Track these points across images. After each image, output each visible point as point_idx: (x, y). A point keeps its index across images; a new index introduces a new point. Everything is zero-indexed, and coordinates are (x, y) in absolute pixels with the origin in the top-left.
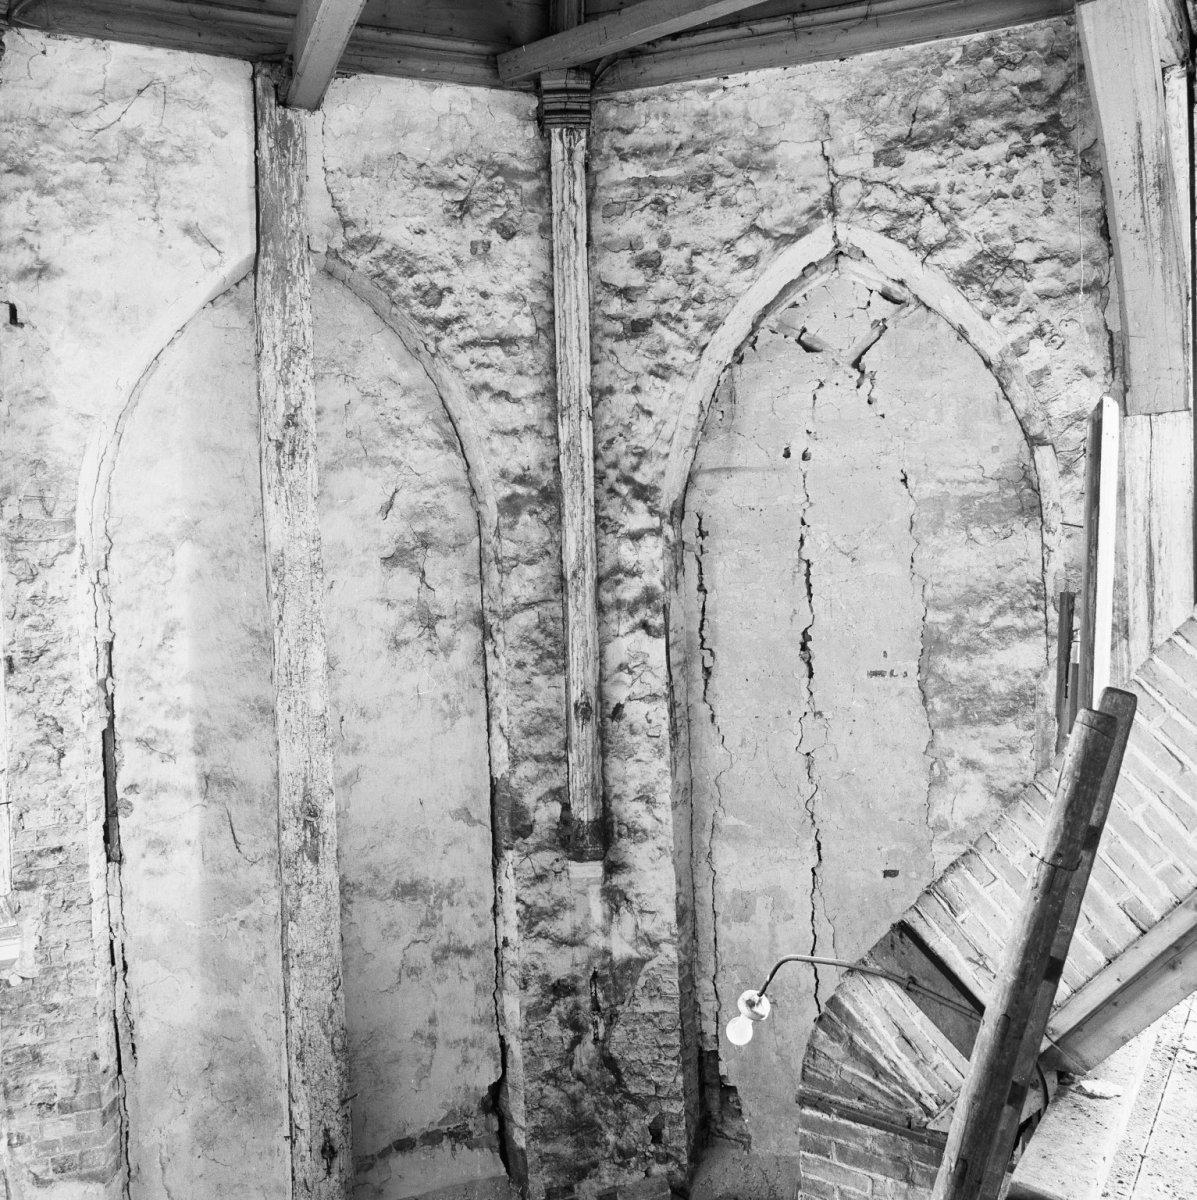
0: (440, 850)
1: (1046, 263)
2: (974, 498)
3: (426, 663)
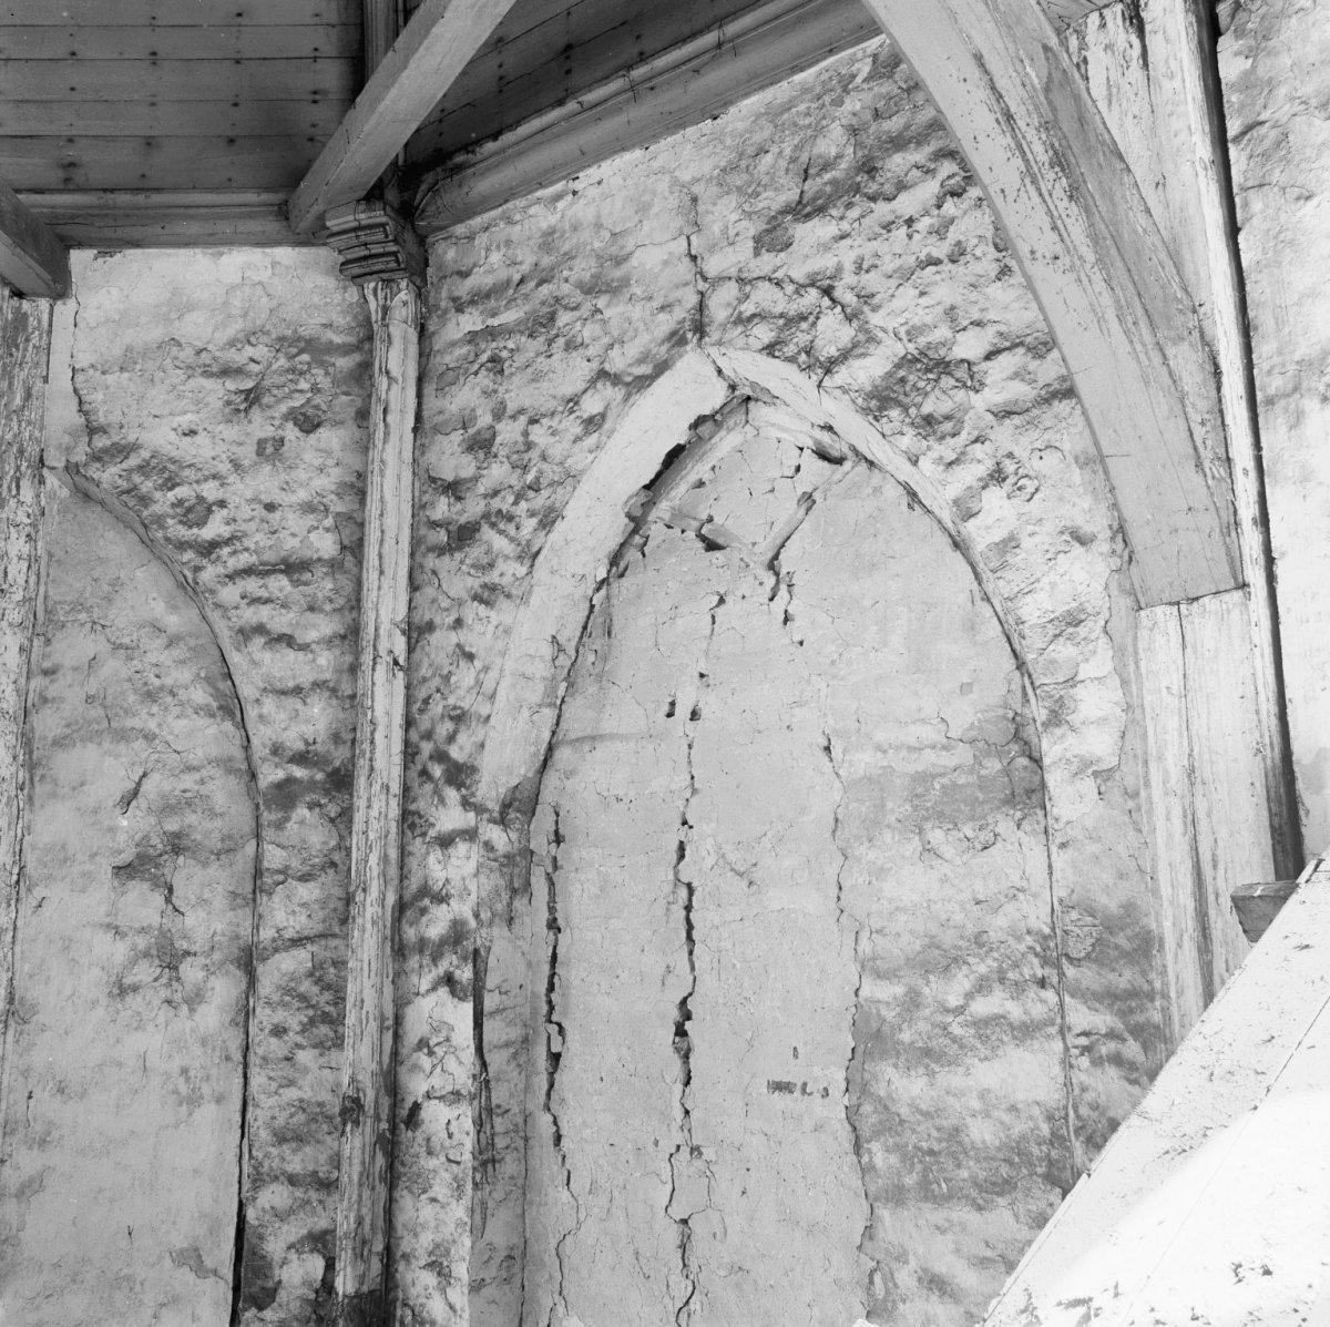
0: (150, 1312)
1: (1003, 358)
2: (934, 777)
3: (161, 1019)
